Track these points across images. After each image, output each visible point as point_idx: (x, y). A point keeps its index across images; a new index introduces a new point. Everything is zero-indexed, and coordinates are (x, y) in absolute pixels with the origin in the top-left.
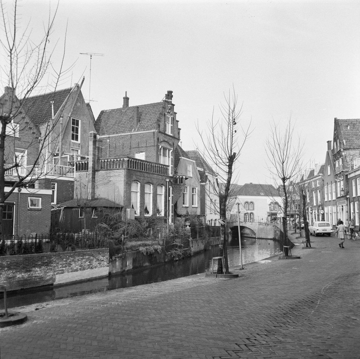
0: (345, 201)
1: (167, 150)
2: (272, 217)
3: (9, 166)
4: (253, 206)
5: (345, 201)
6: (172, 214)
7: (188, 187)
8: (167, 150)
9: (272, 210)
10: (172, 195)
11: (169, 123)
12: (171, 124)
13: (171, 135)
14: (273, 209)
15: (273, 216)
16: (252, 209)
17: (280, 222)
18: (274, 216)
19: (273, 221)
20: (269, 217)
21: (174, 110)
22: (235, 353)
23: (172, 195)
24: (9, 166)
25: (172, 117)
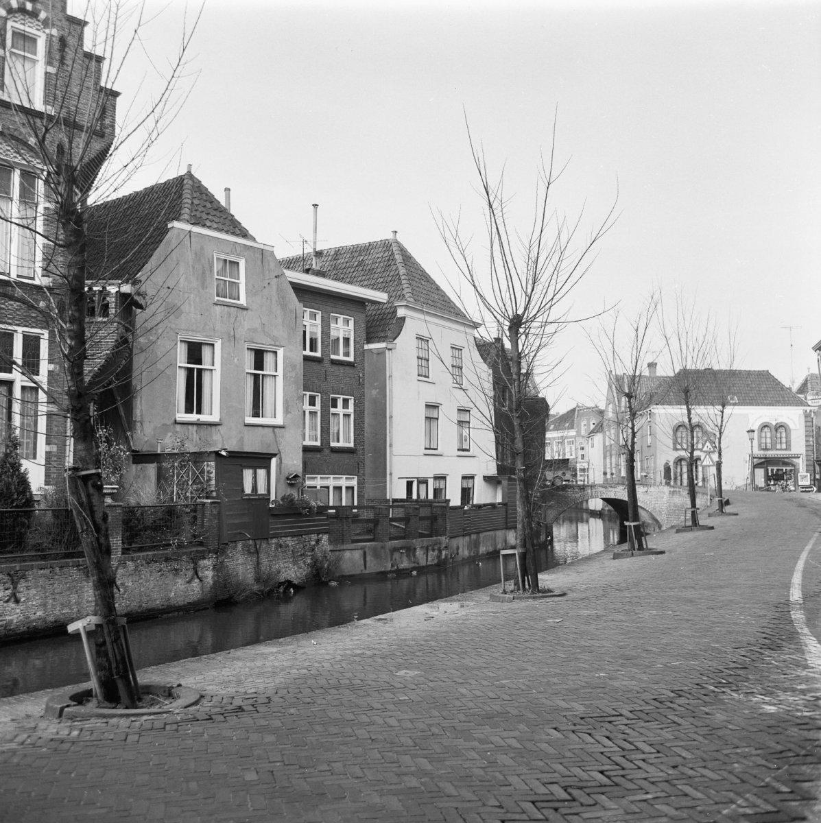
0: (316, 440)
1: (16, 177)
2: (768, 469)
3: (772, 470)
4: (788, 437)
5: (316, 440)
6: (48, 448)
7: (218, 346)
8: (16, 177)
9: (766, 449)
10: (52, 367)
11: (34, 62)
12: (49, 63)
13: (51, 110)
14: (769, 446)
15: (770, 468)
16: (784, 446)
17: (795, 486)
18: (775, 469)
19: (772, 483)
20: (760, 473)
21: (380, 303)
22: (524, 812)
23: (52, 367)
24: (772, 470)
25: (50, 38)
